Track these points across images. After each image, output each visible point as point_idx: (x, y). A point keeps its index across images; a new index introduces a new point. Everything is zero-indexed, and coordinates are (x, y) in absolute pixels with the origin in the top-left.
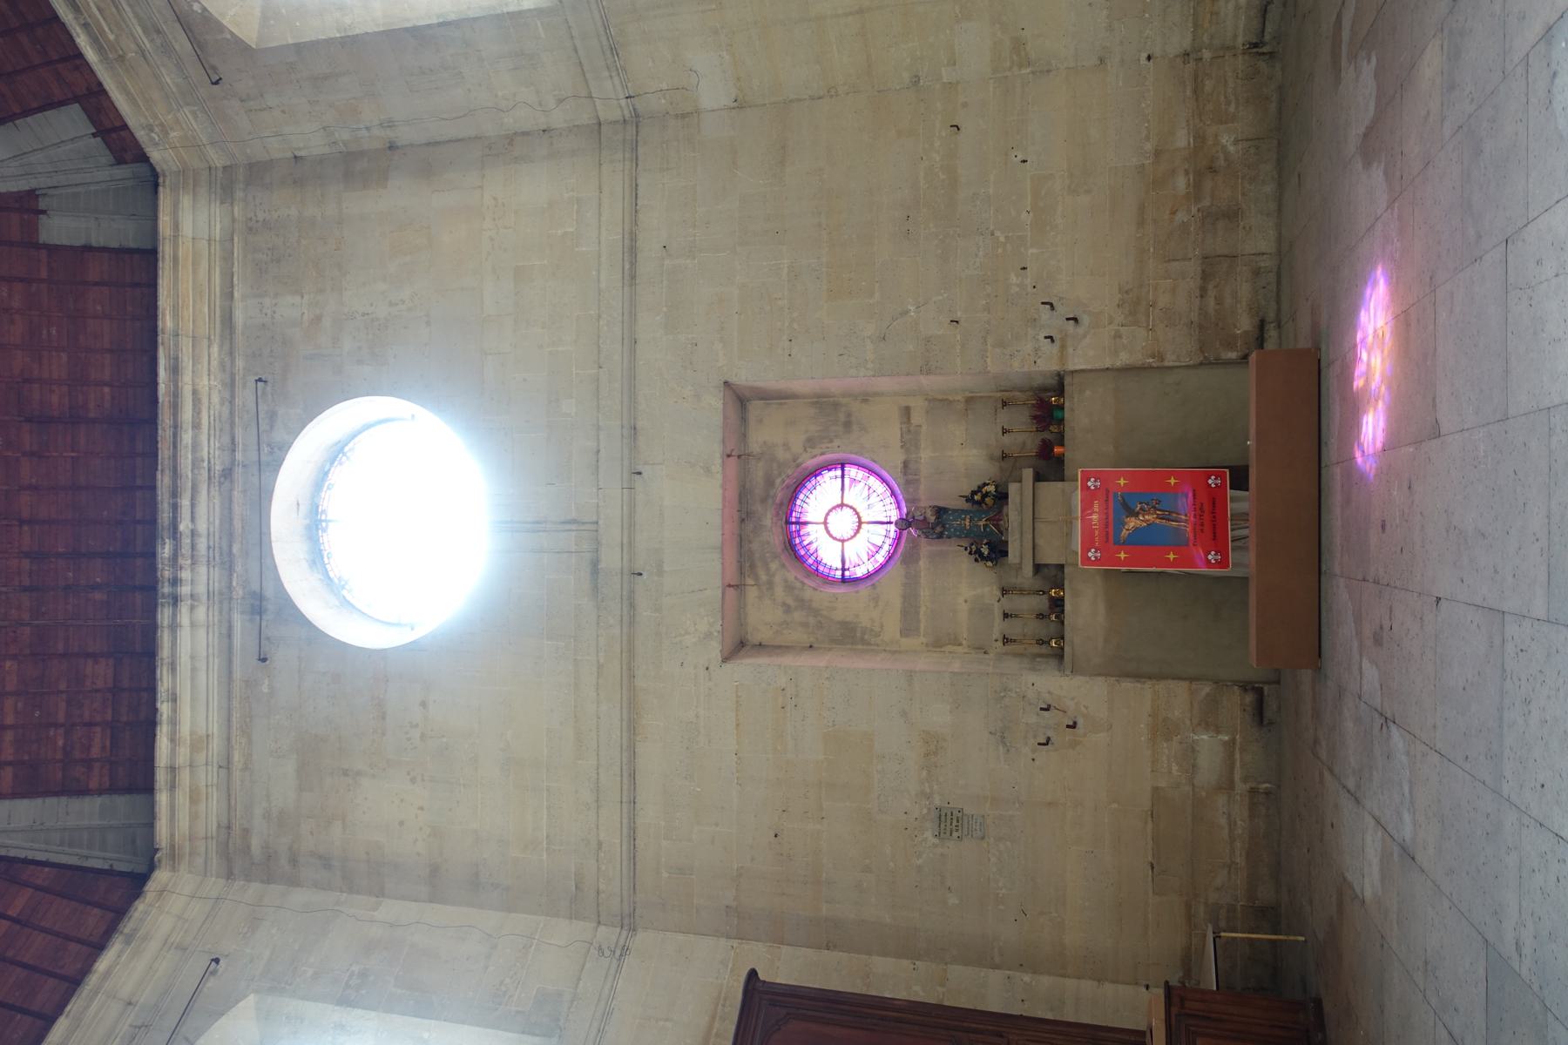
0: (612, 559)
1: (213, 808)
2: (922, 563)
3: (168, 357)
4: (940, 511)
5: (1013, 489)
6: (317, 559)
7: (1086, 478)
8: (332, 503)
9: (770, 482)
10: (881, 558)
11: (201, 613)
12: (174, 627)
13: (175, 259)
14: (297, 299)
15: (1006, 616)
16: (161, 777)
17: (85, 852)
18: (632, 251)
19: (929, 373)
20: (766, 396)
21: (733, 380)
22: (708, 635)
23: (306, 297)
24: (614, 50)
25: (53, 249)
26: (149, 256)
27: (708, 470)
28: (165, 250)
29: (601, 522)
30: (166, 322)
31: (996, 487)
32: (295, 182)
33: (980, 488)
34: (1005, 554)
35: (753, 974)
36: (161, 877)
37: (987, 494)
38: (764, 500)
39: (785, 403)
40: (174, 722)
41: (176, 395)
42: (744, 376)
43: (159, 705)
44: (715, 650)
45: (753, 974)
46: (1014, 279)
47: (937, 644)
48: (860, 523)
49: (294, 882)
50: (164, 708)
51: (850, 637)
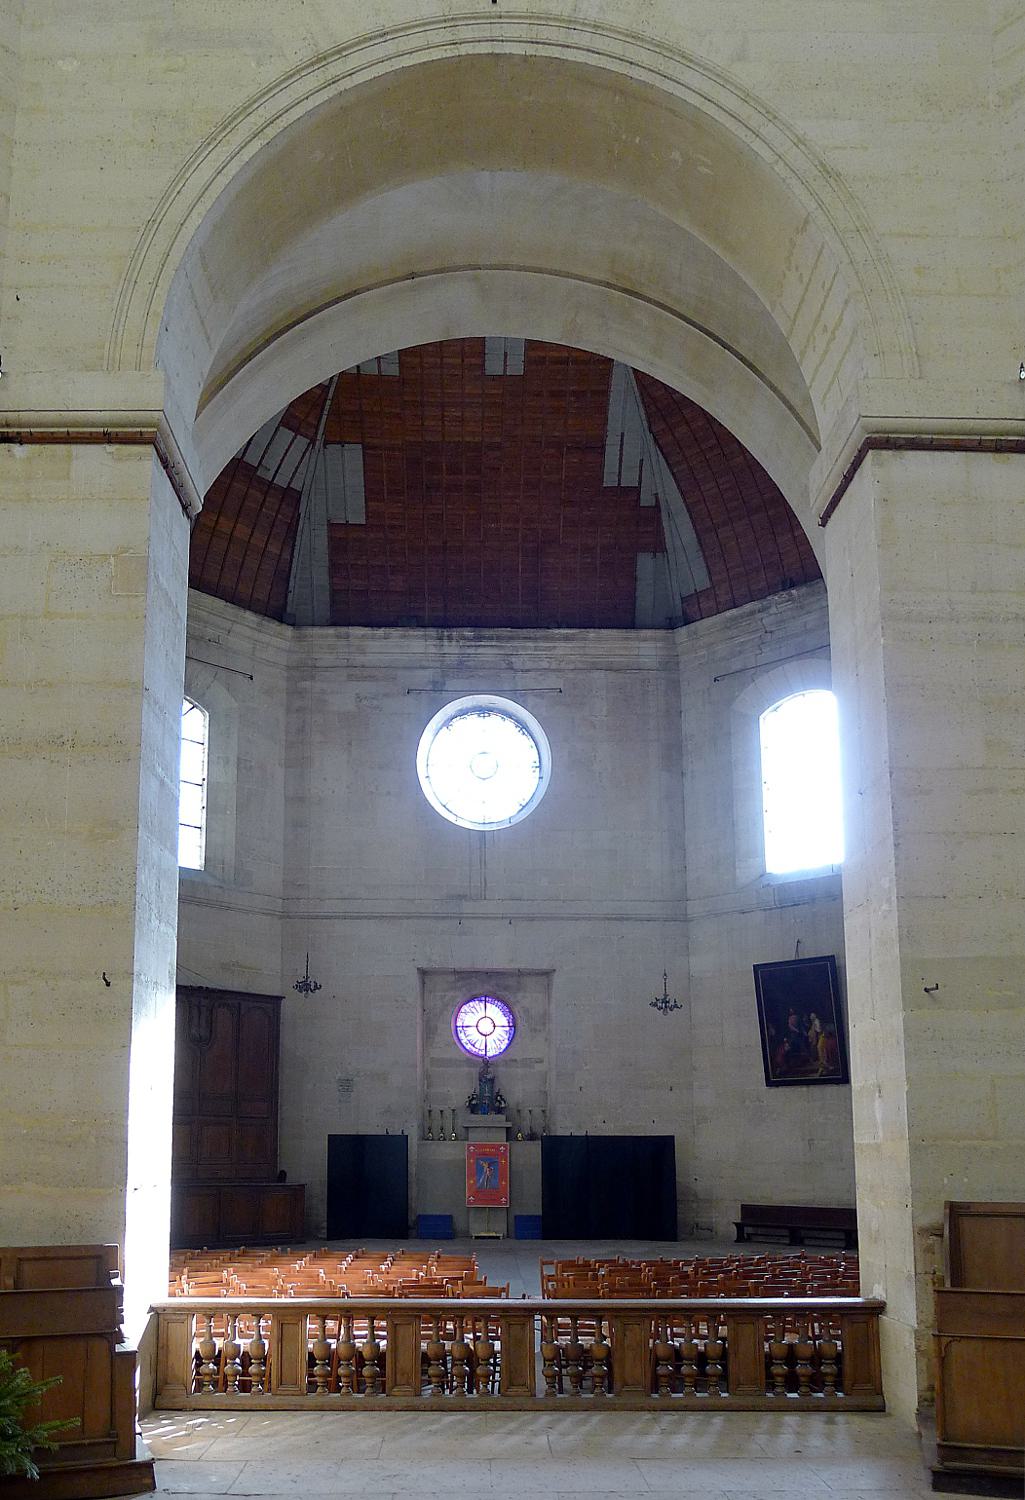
0: (468, 907)
1: (327, 659)
2: (466, 1069)
3: (573, 634)
4: (492, 1080)
5: (503, 1117)
6: (462, 713)
7: (505, 1146)
8: (494, 720)
9: (506, 988)
10: (468, 1047)
11: (434, 650)
12: (425, 638)
13: (627, 639)
14: (604, 713)
15: (442, 1111)
16: (343, 630)
17: (298, 576)
18: (621, 919)
19: (558, 1076)
20: (548, 987)
21: (556, 974)
22: (430, 960)
23: (606, 719)
24: (716, 915)
25: (633, 563)
26: (630, 623)
27: (512, 961)
28: (632, 633)
29: (485, 902)
30: (592, 633)
31: (505, 1108)
32: (668, 711)
33: (502, 1099)
34: (472, 1112)
35: (281, 998)
36: (289, 631)
37: (500, 1103)
38: (497, 985)
39: (376, 1292)
40: (373, 638)
41: (552, 639)
42: (557, 979)
43: (383, 629)
44: (424, 965)
45: (281, 998)
46: (600, 1117)
47: (427, 1076)
48: (486, 1036)
49: (288, 710)
50: (381, 632)
51: (429, 1032)
